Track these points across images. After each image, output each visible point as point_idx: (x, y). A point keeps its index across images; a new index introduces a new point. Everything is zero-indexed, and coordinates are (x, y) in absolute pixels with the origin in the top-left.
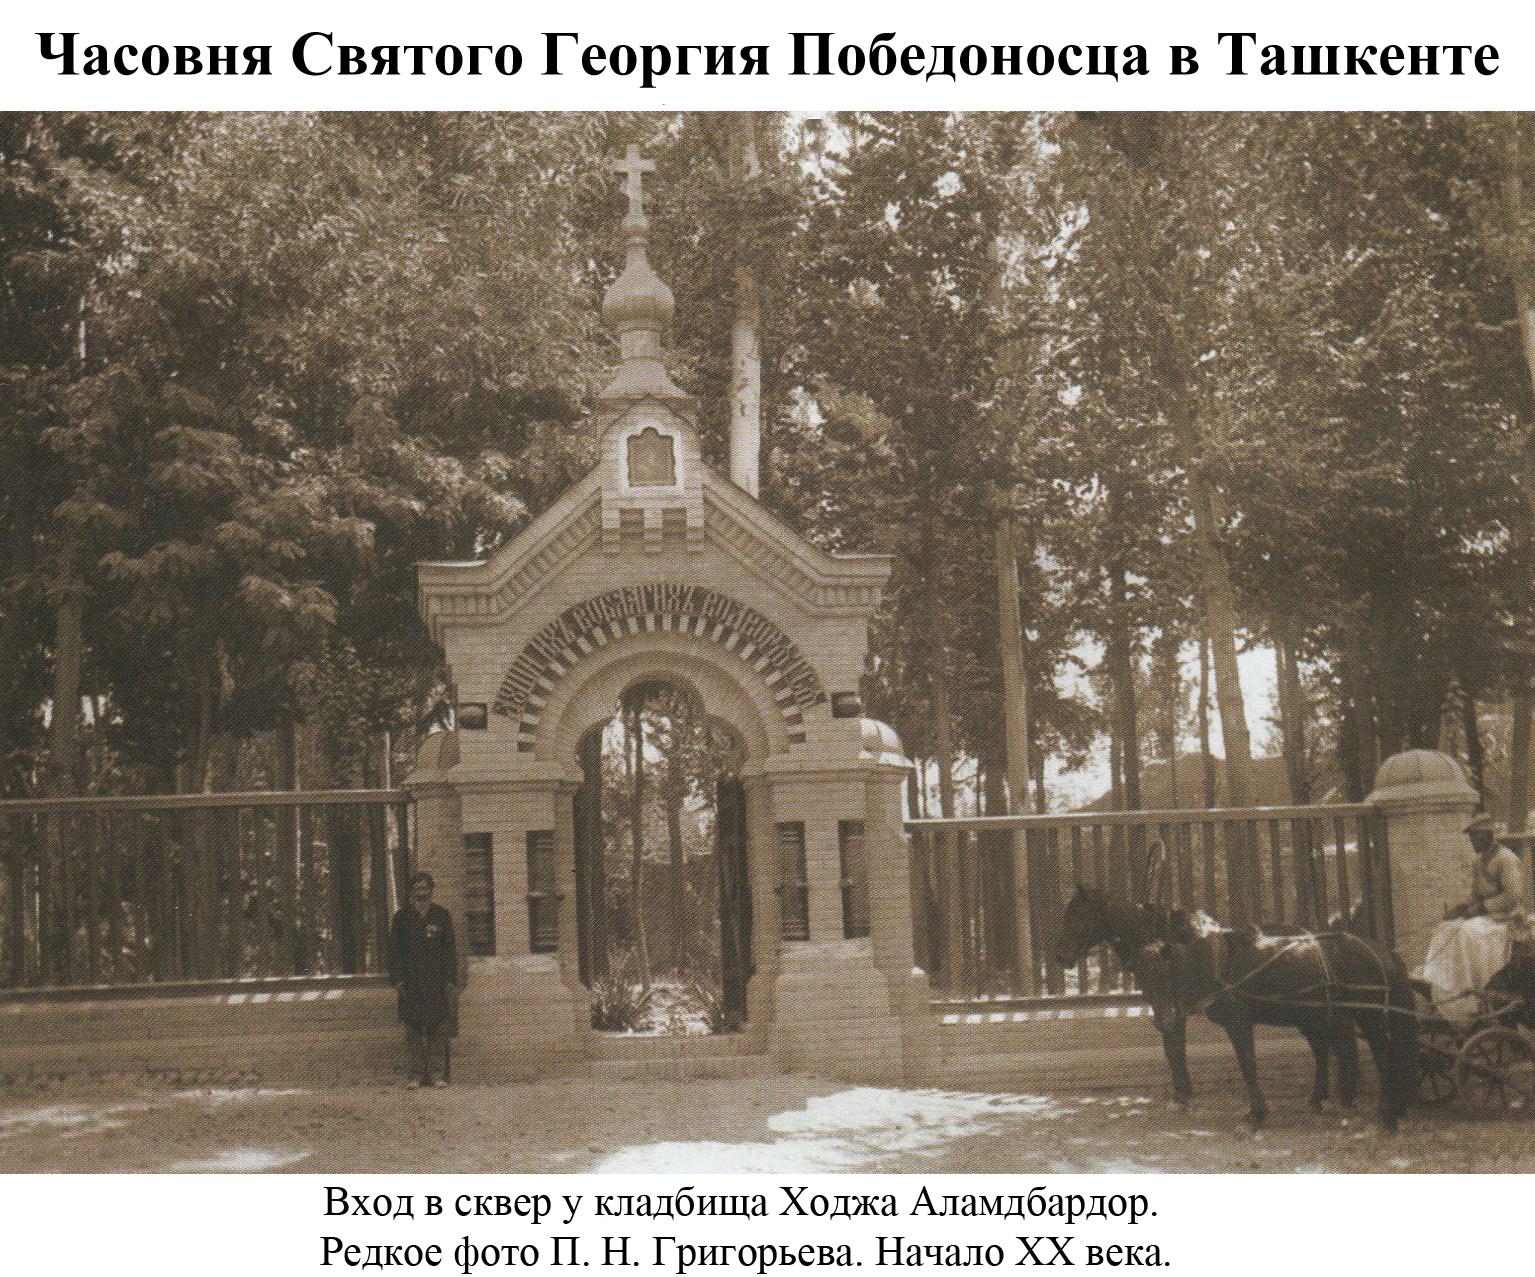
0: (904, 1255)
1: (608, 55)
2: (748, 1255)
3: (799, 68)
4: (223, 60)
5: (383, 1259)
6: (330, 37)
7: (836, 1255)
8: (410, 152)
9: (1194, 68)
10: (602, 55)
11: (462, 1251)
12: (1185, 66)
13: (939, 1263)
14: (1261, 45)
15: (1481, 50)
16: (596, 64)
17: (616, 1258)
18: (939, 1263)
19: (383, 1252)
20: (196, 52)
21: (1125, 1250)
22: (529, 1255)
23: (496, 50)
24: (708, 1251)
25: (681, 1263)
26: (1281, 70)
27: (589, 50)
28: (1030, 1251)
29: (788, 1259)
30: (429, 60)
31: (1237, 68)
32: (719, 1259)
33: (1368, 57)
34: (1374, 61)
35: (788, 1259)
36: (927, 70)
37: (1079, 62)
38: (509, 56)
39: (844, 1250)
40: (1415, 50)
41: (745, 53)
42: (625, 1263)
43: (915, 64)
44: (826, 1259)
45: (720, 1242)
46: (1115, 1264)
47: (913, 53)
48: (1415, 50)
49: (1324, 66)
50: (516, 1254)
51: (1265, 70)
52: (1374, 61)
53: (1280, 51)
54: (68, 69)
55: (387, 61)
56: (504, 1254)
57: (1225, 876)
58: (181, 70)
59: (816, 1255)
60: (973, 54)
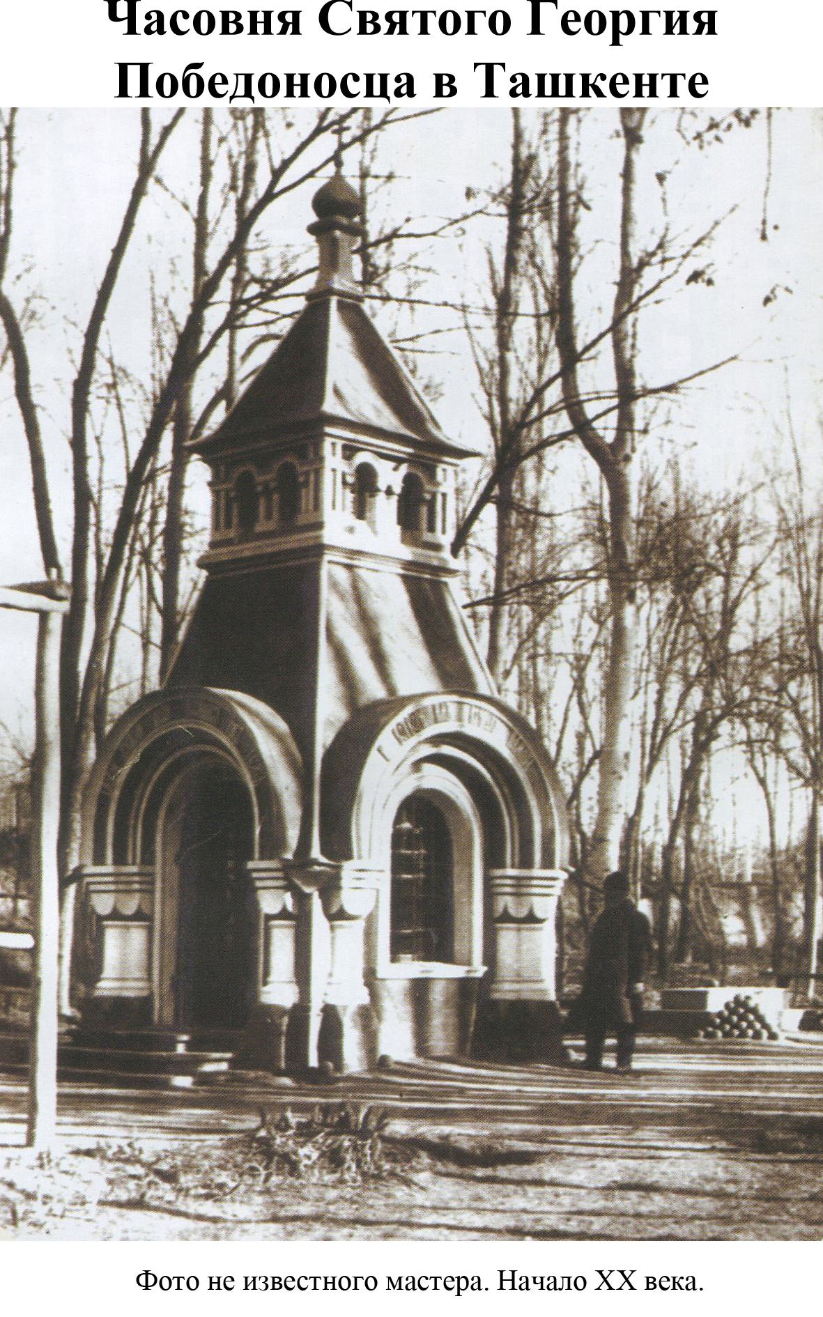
0: (517, 1283)
1: (583, 18)
3: (123, 92)
4: (260, 23)
9: (453, 92)
10: (577, 18)
13: (542, 1288)
14: (511, 71)
16: (573, 26)
18: (542, 1288)
20: (238, 16)
21: (671, 1279)
23: (489, 15)
28: (605, 1280)
30: (433, 22)
31: (490, 92)
33: (599, 83)
34: (604, 86)
36: (230, 94)
40: (639, 77)
41: (697, 16)
43: (220, 89)
47: (218, 79)
48: (639, 77)
52: (604, 86)
53: (525, 78)
54: (132, 30)
55: (398, 24)
56: (175, 1282)
58: (225, 31)
60: (269, 81)
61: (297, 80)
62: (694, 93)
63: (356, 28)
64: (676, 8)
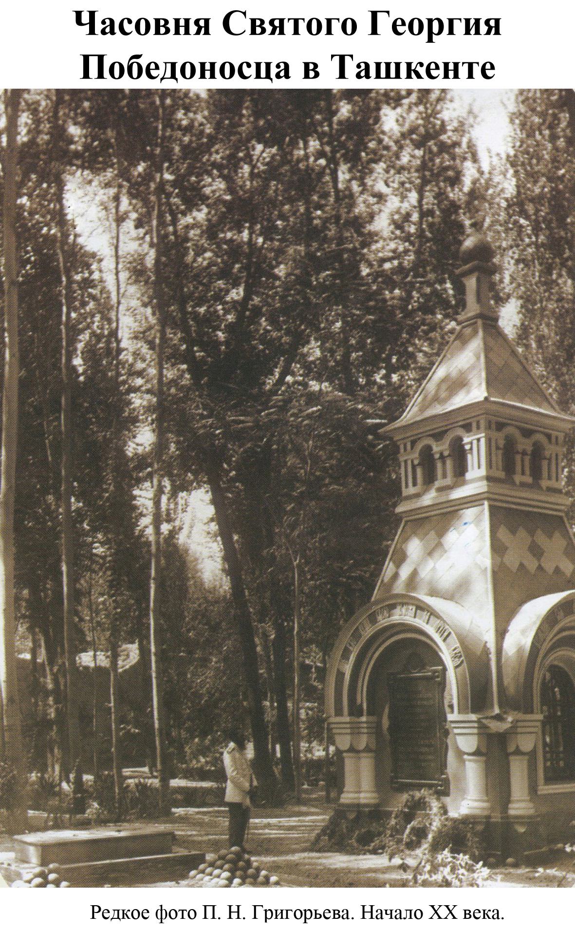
0: (375, 914)
1: (407, 24)
2: (298, 914)
4: (182, 27)
5: (121, 916)
6: (244, 13)
7: (341, 914)
8: (99, 105)
10: (403, 24)
11: (159, 912)
12: (312, 74)
14: (357, 60)
16: (400, 29)
17: (234, 915)
19: (121, 913)
20: (166, 22)
22: (192, 914)
23: (341, 21)
24: (279, 912)
25: (266, 918)
28: (436, 912)
29: (318, 916)
30: (303, 26)
32: (284, 916)
33: (419, 69)
34: (422, 71)
35: (318, 916)
36: (161, 76)
39: (345, 912)
40: (446, 65)
42: (238, 918)
43: (154, 73)
44: (337, 916)
45: (285, 908)
46: (477, 918)
47: (153, 66)
48: (446, 65)
49: (393, 73)
50: (185, 913)
52: (422, 71)
53: (367, 66)
54: (92, 32)
55: (278, 27)
56: (180, 914)
58: (157, 32)
59: (332, 914)
61: (208, 67)
62: (485, 76)
63: (249, 30)
64: (472, 16)
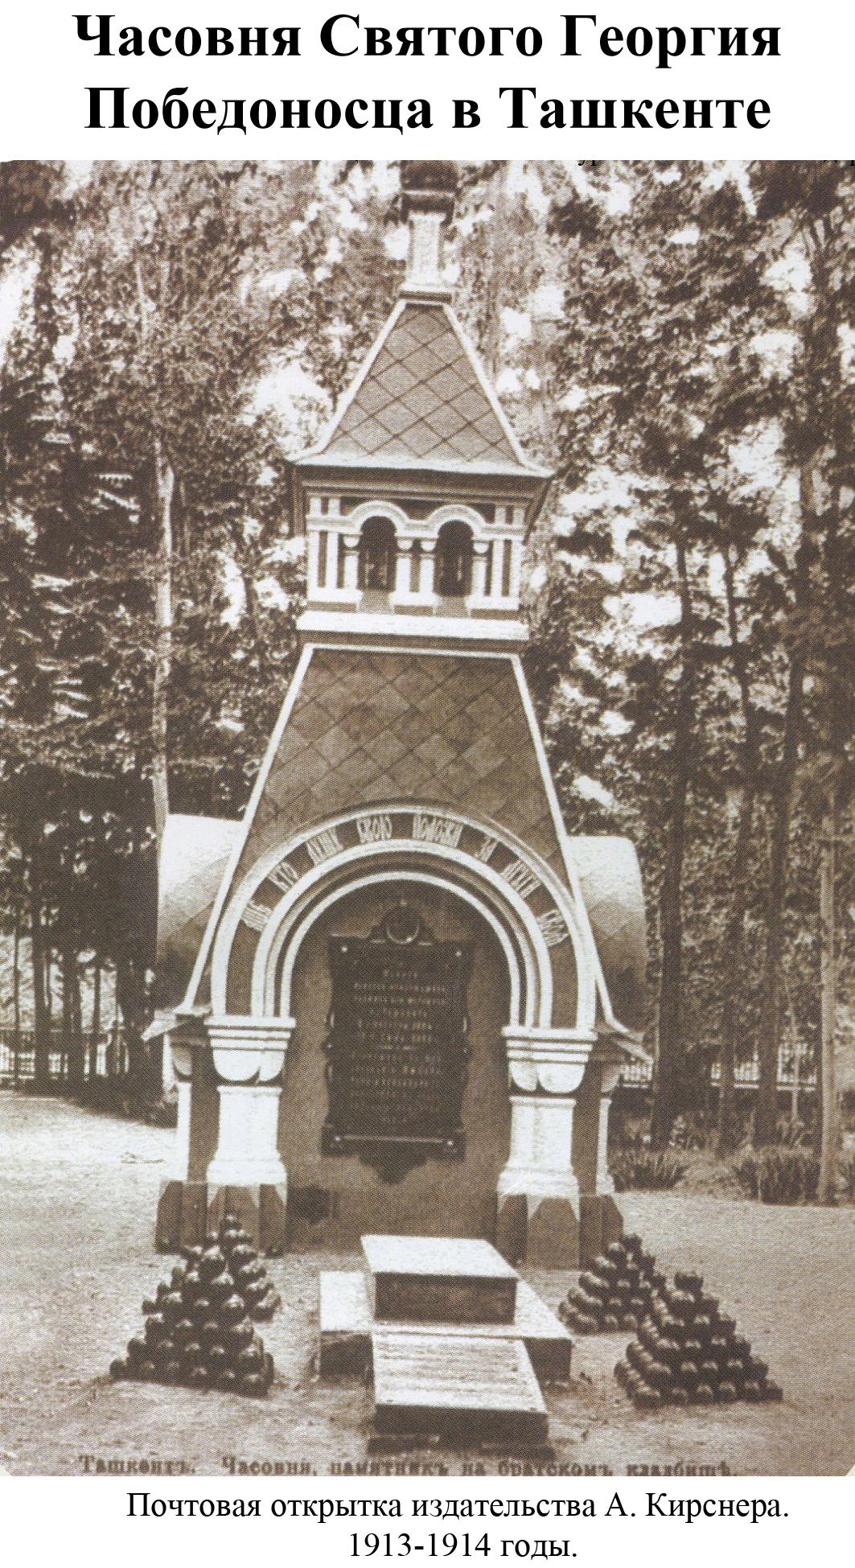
1: (625, 36)
3: (95, 122)
4: (253, 41)
6: (356, 20)
9: (476, 121)
10: (619, 37)
12: (468, 120)
15: (753, 105)
16: (614, 46)
19: (548, 1546)
20: (228, 34)
23: (516, 32)
26: (560, 123)
27: (606, 33)
30: (452, 41)
31: (518, 122)
33: (644, 111)
34: (650, 115)
36: (218, 124)
37: (366, 116)
38: (529, 38)
40: (690, 105)
41: (757, 34)
43: (207, 118)
47: (205, 107)
48: (690, 105)
49: (601, 119)
51: (545, 123)
52: (650, 115)
53: (559, 105)
54: (105, 50)
55: (412, 42)
57: (780, 1052)
58: (213, 51)
62: (754, 123)
64: (733, 25)
